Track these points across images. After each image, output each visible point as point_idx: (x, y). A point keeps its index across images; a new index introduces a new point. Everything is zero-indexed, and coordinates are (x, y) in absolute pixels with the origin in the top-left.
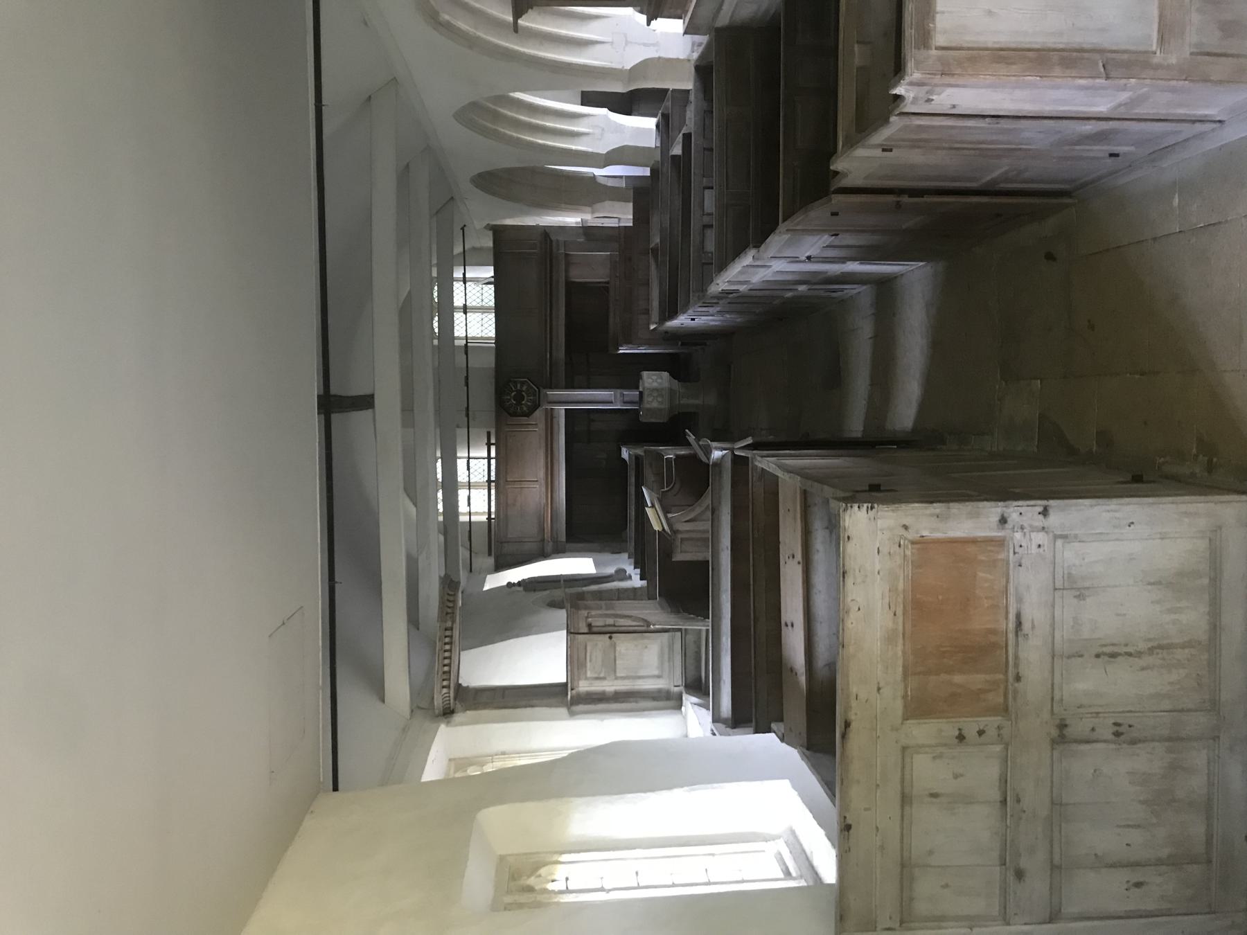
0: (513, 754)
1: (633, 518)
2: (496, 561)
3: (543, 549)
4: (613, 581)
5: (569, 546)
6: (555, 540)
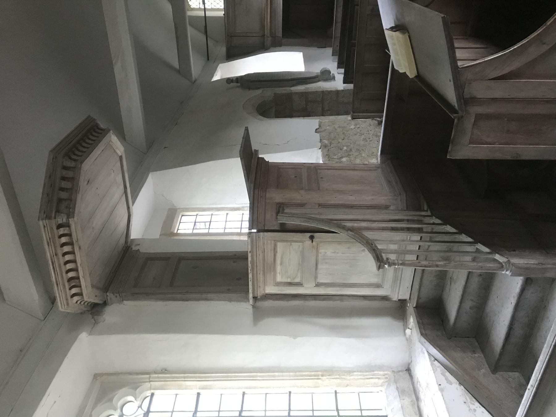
0: (176, 373)
1: (340, 19)
2: (228, 50)
3: (263, 43)
4: (319, 81)
5: (284, 41)
6: (273, 35)
